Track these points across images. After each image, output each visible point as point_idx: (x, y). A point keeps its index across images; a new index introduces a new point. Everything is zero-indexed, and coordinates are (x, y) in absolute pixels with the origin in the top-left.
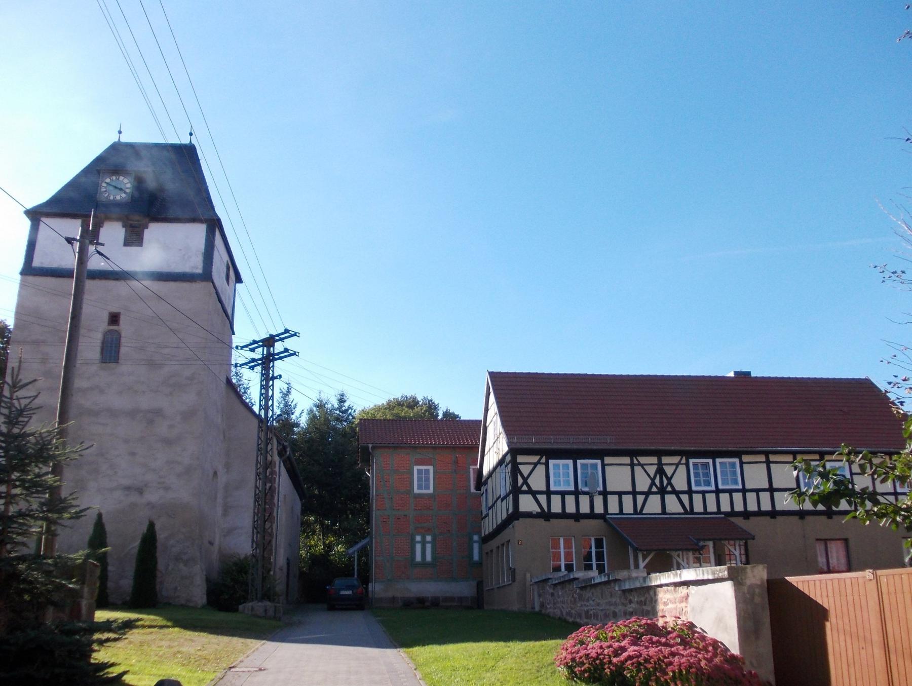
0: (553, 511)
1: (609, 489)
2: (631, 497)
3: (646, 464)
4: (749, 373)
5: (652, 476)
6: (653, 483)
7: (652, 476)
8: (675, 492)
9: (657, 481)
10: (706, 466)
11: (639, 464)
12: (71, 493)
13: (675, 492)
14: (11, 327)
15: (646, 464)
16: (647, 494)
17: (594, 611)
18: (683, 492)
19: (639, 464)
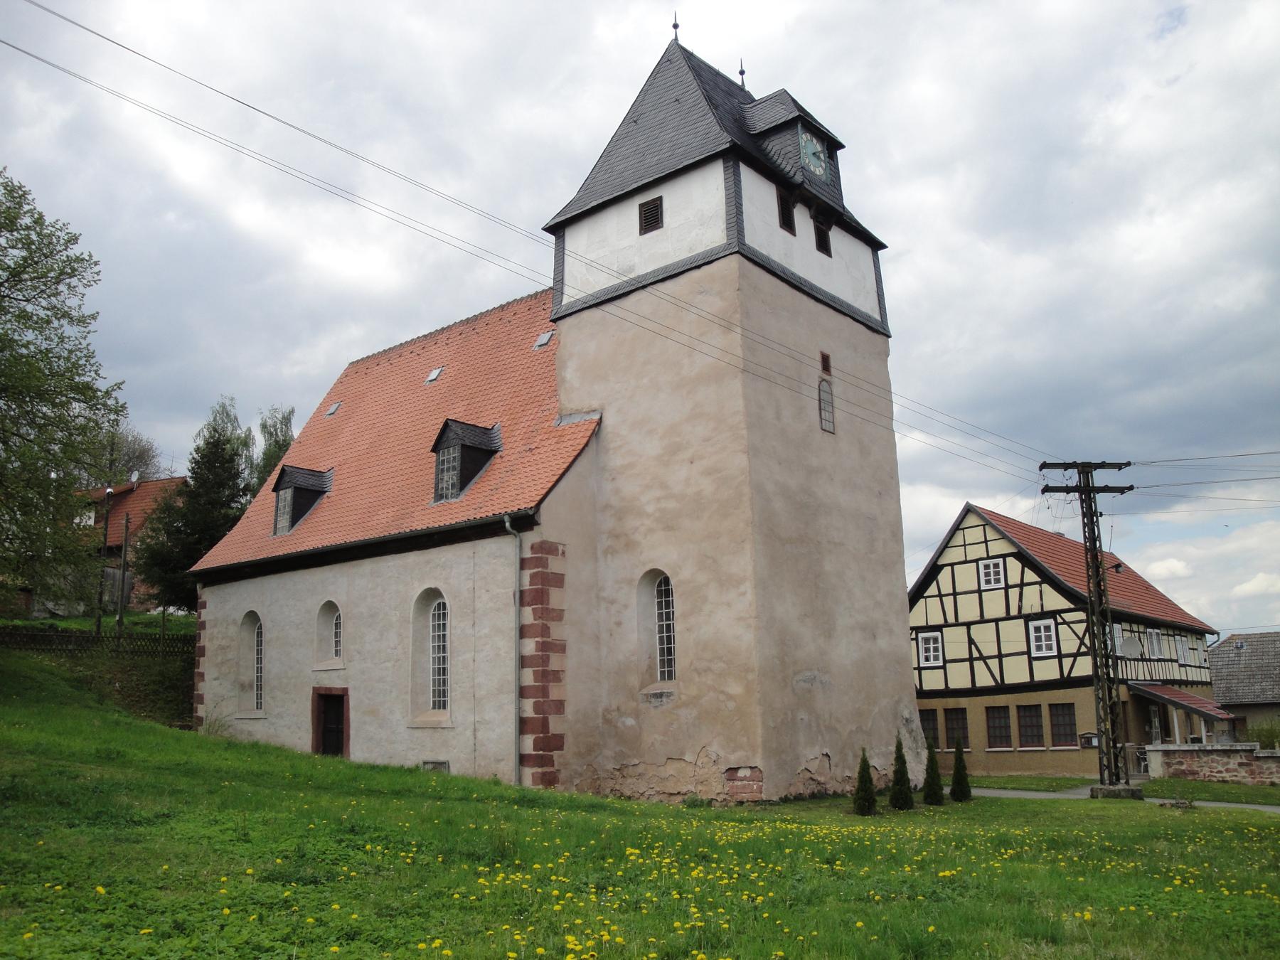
0: (1007, 681)
1: (967, 656)
2: (997, 660)
3: (1073, 622)
4: (204, 656)
5: (1081, 636)
6: (1082, 643)
7: (1081, 636)
8: (983, 658)
9: (1087, 641)
10: (1047, 628)
11: (1065, 623)
12: (833, 363)
13: (983, 658)
14: (296, 437)
15: (1073, 622)
16: (1075, 656)
17: (886, 893)
18: (977, 659)
19: (1065, 623)
